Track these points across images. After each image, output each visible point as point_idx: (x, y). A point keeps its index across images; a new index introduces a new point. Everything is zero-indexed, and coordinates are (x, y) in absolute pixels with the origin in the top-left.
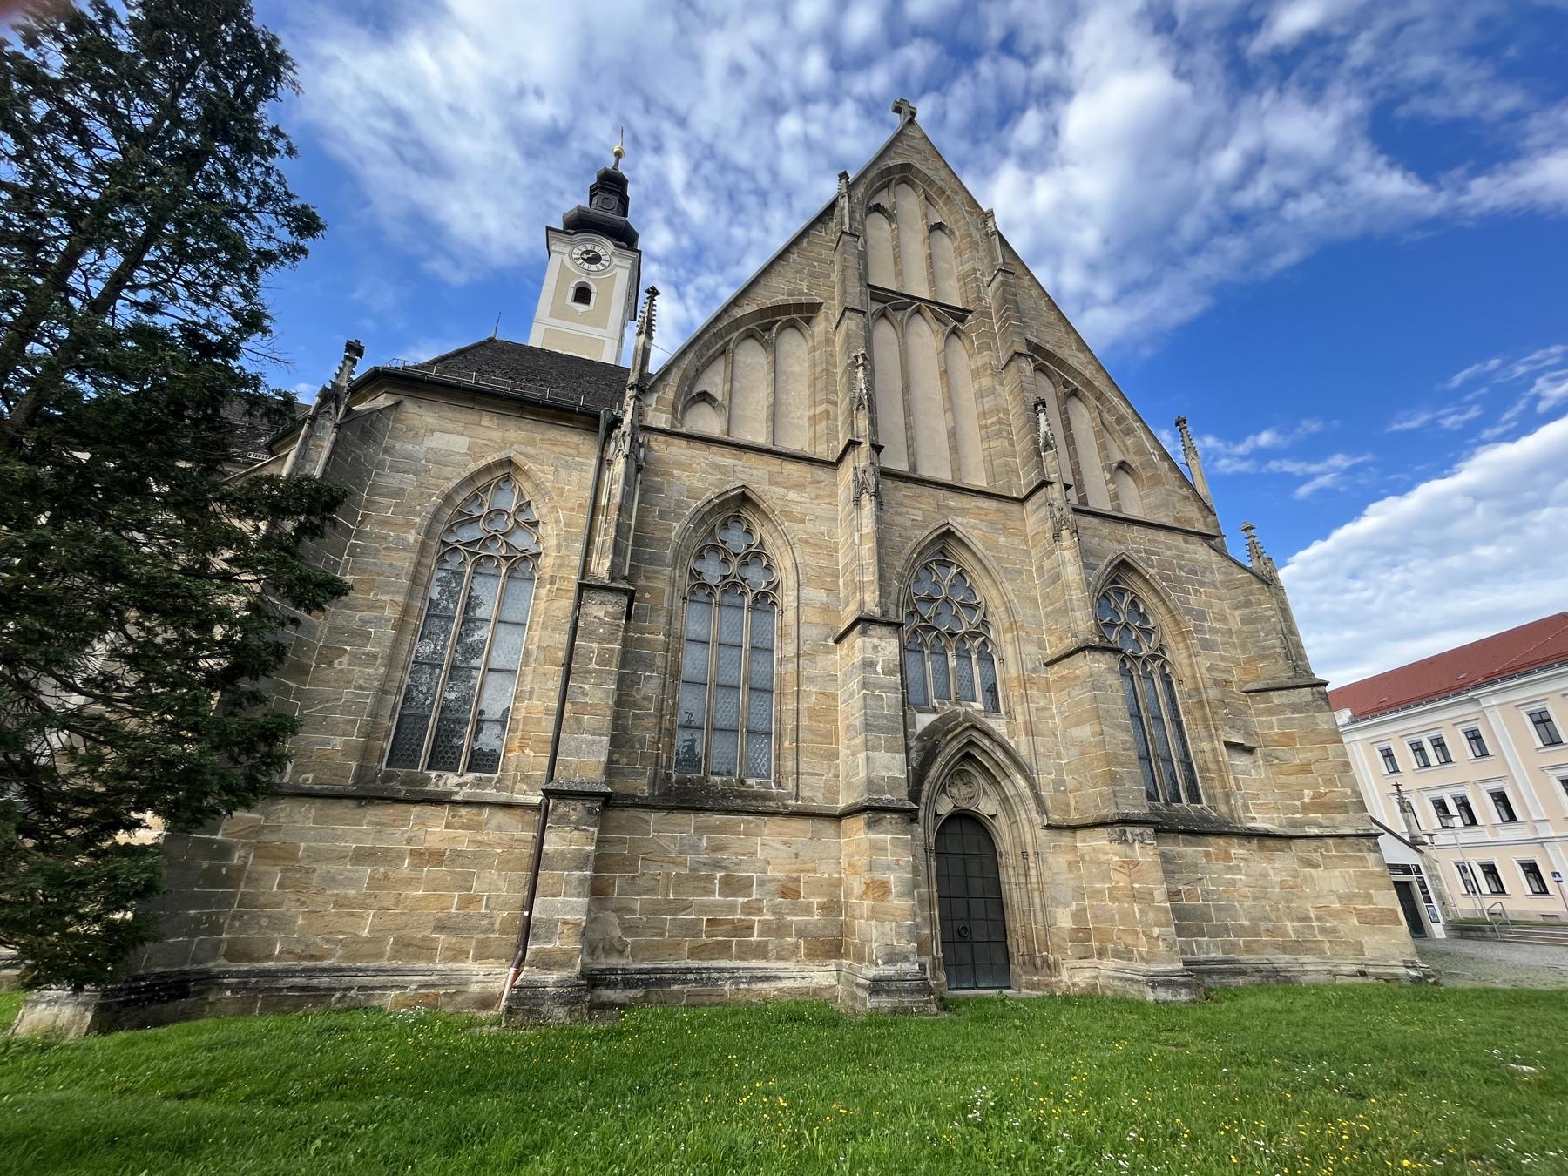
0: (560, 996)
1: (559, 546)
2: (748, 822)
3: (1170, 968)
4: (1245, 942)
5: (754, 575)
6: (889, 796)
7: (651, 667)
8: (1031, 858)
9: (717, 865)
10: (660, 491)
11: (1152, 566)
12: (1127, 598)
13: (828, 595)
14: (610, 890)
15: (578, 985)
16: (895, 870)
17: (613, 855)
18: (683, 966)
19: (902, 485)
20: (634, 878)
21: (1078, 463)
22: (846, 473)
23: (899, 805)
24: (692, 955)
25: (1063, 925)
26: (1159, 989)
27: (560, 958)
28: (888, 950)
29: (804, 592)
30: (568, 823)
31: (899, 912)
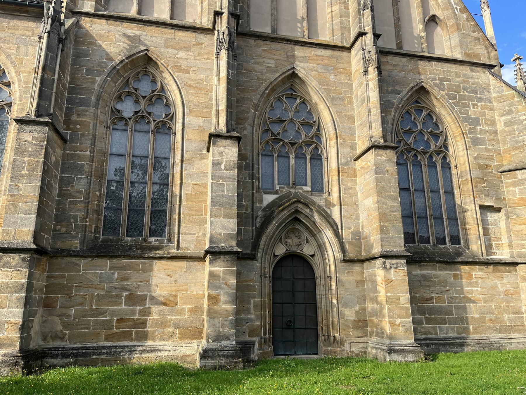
0: (5, 361)
1: (20, 96)
2: (144, 263)
4: (473, 327)
5: (158, 111)
6: (223, 245)
7: (81, 172)
9: (124, 289)
10: (87, 55)
11: (443, 90)
12: (424, 113)
13: (203, 121)
14: (55, 304)
15: (17, 356)
17: (56, 285)
18: (101, 345)
19: (261, 42)
20: (70, 297)
21: (399, 18)
22: (356, 55)
23: (230, 249)
24: (107, 339)
25: (349, 318)
26: (393, 354)
27: (7, 342)
29: (187, 119)
30: (10, 267)
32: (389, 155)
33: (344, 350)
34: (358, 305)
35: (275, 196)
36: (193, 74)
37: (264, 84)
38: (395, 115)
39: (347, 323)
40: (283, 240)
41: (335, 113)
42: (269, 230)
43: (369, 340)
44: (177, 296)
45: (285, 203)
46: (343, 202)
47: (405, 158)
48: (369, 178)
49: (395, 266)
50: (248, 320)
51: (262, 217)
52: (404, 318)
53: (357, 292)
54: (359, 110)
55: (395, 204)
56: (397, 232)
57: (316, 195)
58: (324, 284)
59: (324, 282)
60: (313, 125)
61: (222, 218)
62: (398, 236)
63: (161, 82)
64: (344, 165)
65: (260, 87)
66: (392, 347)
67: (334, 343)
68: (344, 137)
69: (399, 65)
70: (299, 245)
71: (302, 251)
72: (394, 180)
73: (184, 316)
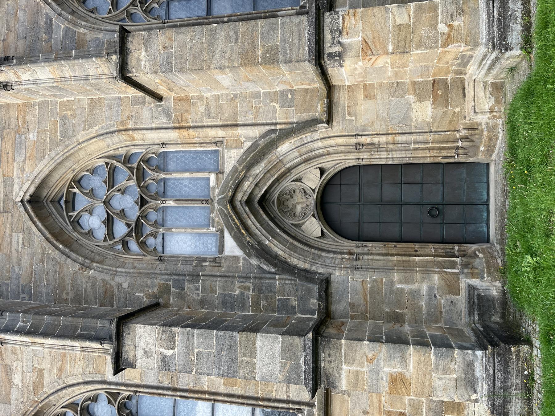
3: (483, 16)
6: (302, 360)
8: (362, 140)
16: (378, 365)
25: (430, 114)
26: (509, 41)
28: (461, 385)
31: (422, 366)
32: (137, 46)
33: (487, 124)
34: (407, 97)
35: (227, 234)
36: (43, 364)
37: (50, 252)
38: (85, 28)
39: (438, 118)
40: (297, 222)
41: (87, 132)
42: (280, 252)
43: (471, 77)
44: (389, 412)
45: (235, 224)
46: (230, 120)
47: (156, 6)
48: (183, 80)
49: (336, 34)
50: (431, 296)
51: (260, 261)
52: (437, 16)
53: (382, 98)
54: (76, 93)
55: (223, 34)
56: (273, 30)
57: (223, 165)
58: (368, 154)
59: (366, 154)
60: (113, 167)
61: (255, 360)
62: (282, 28)
63: (62, 407)
64: (170, 119)
65: (54, 259)
66: (493, 43)
67: (473, 141)
68: (125, 117)
69: (7, 20)
70: (305, 193)
71: (314, 190)
72: (181, 36)
73: (423, 402)
